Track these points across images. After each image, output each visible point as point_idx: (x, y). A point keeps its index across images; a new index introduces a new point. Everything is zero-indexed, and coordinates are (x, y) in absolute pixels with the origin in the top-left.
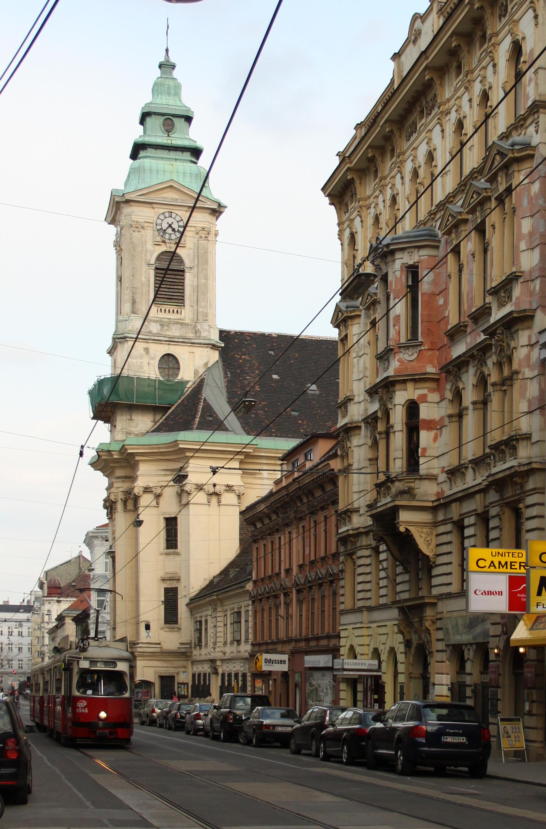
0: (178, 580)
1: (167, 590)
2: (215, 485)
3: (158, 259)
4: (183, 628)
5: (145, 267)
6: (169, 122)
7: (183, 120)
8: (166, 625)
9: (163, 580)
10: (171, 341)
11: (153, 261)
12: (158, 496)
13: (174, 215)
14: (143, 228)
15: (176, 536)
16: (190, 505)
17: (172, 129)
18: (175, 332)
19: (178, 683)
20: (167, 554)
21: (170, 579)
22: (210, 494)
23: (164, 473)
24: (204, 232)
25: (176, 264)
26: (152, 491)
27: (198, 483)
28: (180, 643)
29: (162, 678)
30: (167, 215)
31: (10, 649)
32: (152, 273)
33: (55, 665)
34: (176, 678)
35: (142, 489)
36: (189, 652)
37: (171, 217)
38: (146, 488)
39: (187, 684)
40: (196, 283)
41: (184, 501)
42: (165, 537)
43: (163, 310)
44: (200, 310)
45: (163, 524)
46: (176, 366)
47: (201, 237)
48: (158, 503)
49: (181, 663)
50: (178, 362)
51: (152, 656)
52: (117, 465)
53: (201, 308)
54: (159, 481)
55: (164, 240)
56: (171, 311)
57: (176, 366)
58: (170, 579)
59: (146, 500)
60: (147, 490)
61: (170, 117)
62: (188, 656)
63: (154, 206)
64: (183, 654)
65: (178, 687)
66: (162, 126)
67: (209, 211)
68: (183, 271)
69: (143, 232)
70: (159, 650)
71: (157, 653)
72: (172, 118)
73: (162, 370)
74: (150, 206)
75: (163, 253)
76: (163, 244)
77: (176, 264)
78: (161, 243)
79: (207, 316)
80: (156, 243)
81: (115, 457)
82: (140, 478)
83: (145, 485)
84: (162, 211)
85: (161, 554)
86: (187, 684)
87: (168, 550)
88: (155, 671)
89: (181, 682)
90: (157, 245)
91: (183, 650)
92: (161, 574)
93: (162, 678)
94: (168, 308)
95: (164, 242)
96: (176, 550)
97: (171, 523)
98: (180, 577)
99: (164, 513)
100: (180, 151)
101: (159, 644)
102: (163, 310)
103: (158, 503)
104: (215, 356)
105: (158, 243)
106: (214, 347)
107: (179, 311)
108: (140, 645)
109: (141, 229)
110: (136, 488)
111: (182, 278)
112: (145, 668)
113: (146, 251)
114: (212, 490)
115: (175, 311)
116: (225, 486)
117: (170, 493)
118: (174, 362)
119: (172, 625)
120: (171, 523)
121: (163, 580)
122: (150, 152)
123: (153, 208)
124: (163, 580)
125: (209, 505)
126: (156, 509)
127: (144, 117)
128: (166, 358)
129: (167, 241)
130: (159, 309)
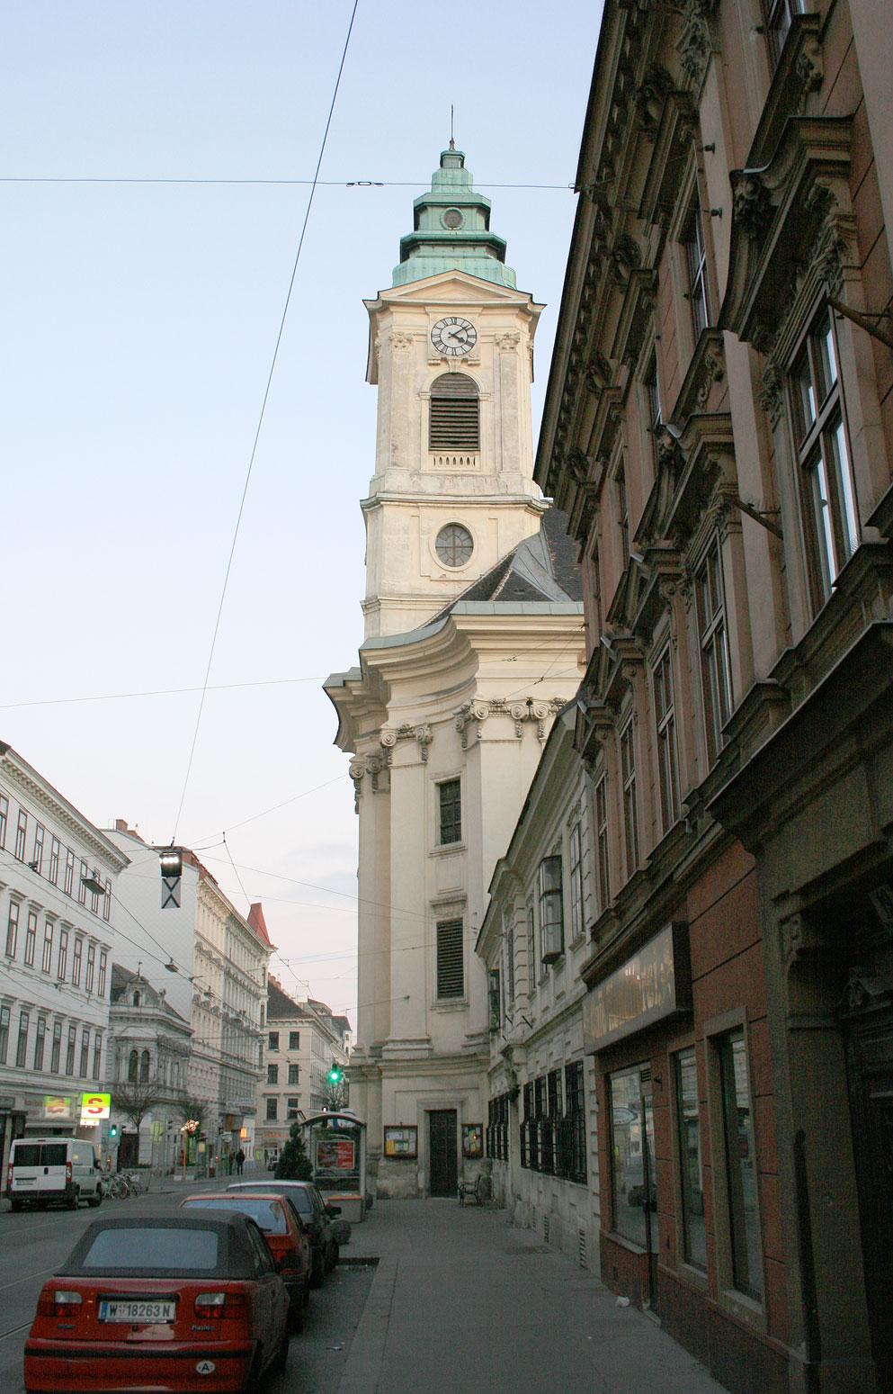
0: (464, 901)
1: (442, 928)
2: (529, 703)
3: (435, 385)
4: (472, 1003)
5: (413, 398)
6: (455, 215)
7: (475, 210)
8: (442, 1001)
9: (434, 906)
10: (455, 504)
11: (427, 387)
12: (425, 743)
13: (459, 322)
14: (410, 341)
15: (458, 817)
16: (483, 746)
17: (459, 223)
18: (464, 488)
19: (464, 1126)
20: (442, 854)
21: (448, 903)
22: (522, 720)
23: (434, 698)
24: (508, 341)
25: (465, 390)
26: (414, 736)
27: (496, 699)
28: (468, 1036)
29: (433, 1114)
30: (449, 321)
31: (110, 1051)
32: (425, 407)
33: (510, 1171)
34: (459, 1116)
35: (394, 735)
36: (482, 1053)
37: (455, 324)
38: (402, 731)
39: (481, 1126)
40: (497, 415)
41: (472, 740)
42: (439, 822)
43: (444, 459)
44: (505, 454)
45: (433, 796)
46: (466, 543)
47: (503, 348)
48: (425, 758)
49: (466, 1080)
50: (470, 538)
51: (411, 1066)
52: (363, 712)
53: (507, 450)
54: (426, 716)
55: (444, 356)
56: (458, 460)
57: (466, 543)
58: (448, 903)
59: (404, 754)
60: (404, 734)
61: (455, 208)
62: (481, 1063)
63: (428, 309)
64: (471, 1059)
65: (464, 1135)
66: (442, 220)
67: (517, 311)
68: (476, 400)
69: (410, 348)
70: (426, 1054)
71: (421, 1060)
72: (457, 209)
73: (443, 551)
74: (421, 311)
75: (442, 377)
76: (443, 364)
77: (465, 390)
78: (439, 362)
79: (517, 463)
80: (432, 362)
81: (355, 693)
82: (391, 714)
83: (399, 727)
84: (441, 317)
85: (431, 856)
86: (481, 1126)
87: (444, 846)
88: (419, 1102)
89: (469, 1122)
90: (433, 364)
91: (472, 1050)
92: (433, 895)
93: (433, 1114)
94: (451, 455)
95: (445, 360)
96: (458, 843)
97: (449, 790)
98: (466, 896)
99: (436, 774)
100: (470, 245)
101: (428, 1041)
102: (444, 459)
103: (425, 758)
104: (533, 525)
105: (436, 362)
106: (529, 506)
107: (471, 460)
108: (390, 1046)
109: (407, 344)
110: (383, 732)
111: (476, 410)
112: (398, 1094)
113: (416, 376)
114: (524, 711)
115: (465, 460)
116: (551, 702)
117: (446, 739)
118: (464, 536)
119: (452, 999)
120: (449, 790)
121: (435, 906)
122: (424, 250)
123: (427, 314)
124: (434, 906)
125: (520, 742)
126: (421, 769)
127: (420, 209)
128: (450, 531)
129: (449, 358)
130: (437, 459)
